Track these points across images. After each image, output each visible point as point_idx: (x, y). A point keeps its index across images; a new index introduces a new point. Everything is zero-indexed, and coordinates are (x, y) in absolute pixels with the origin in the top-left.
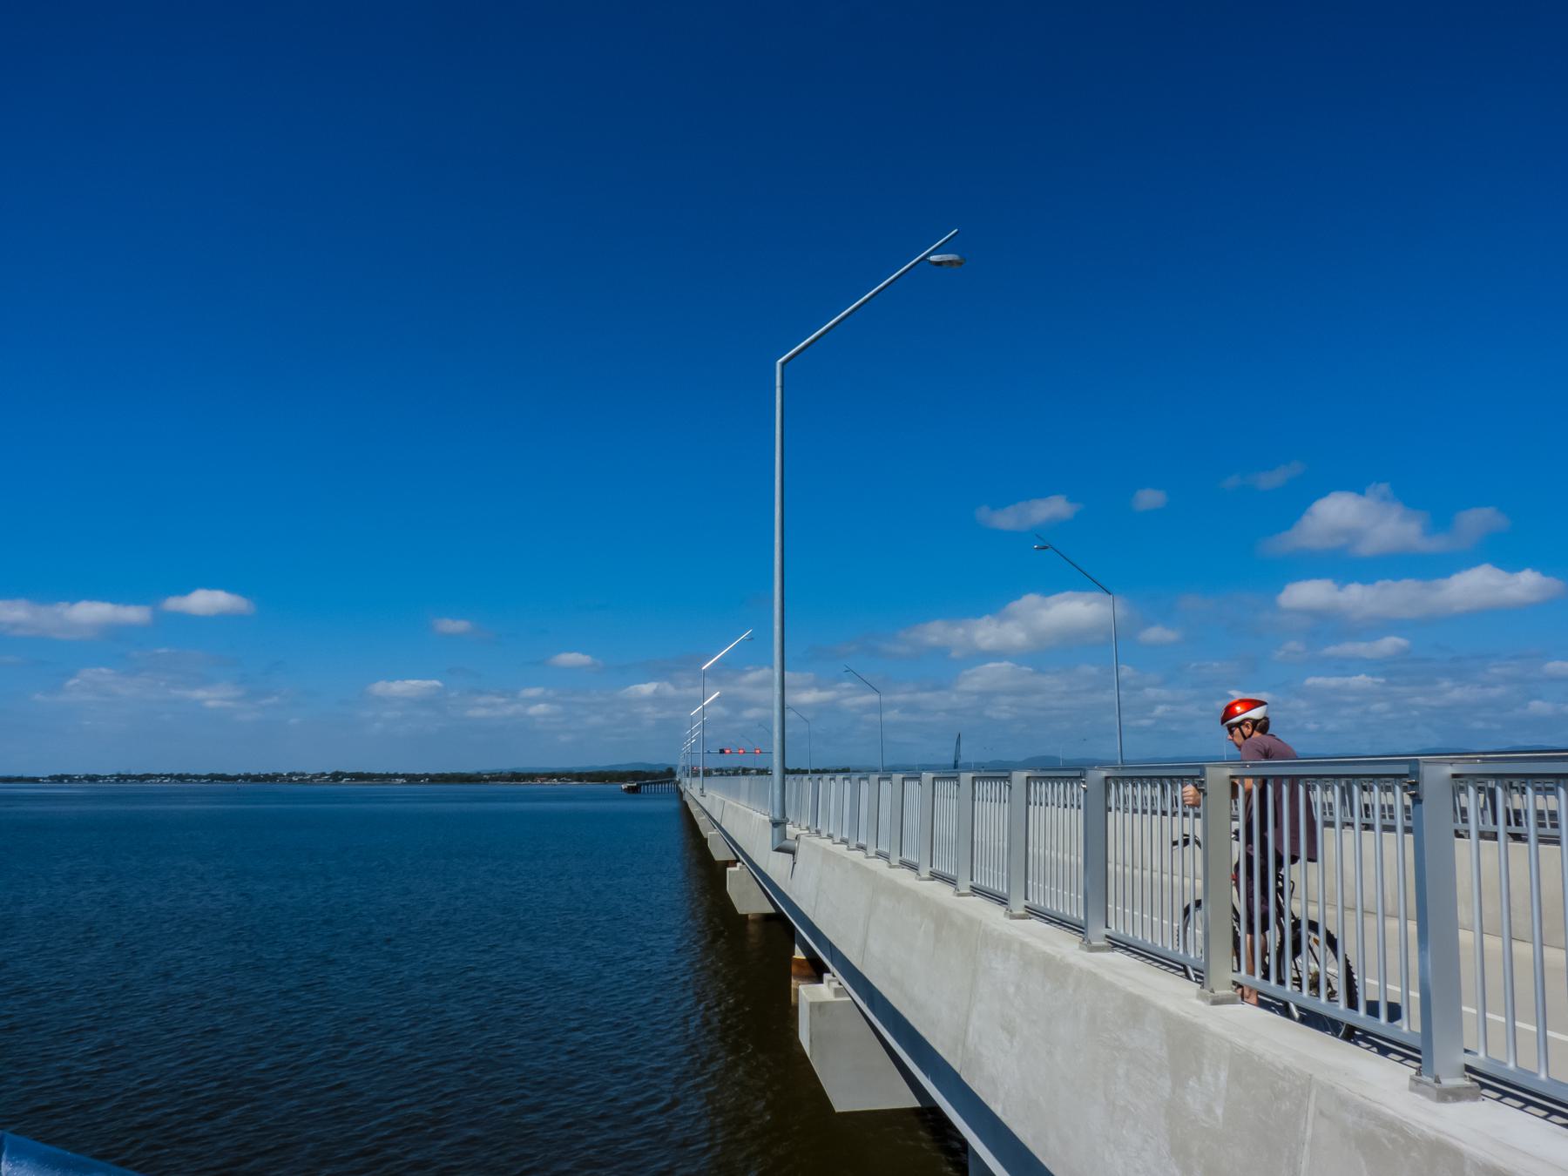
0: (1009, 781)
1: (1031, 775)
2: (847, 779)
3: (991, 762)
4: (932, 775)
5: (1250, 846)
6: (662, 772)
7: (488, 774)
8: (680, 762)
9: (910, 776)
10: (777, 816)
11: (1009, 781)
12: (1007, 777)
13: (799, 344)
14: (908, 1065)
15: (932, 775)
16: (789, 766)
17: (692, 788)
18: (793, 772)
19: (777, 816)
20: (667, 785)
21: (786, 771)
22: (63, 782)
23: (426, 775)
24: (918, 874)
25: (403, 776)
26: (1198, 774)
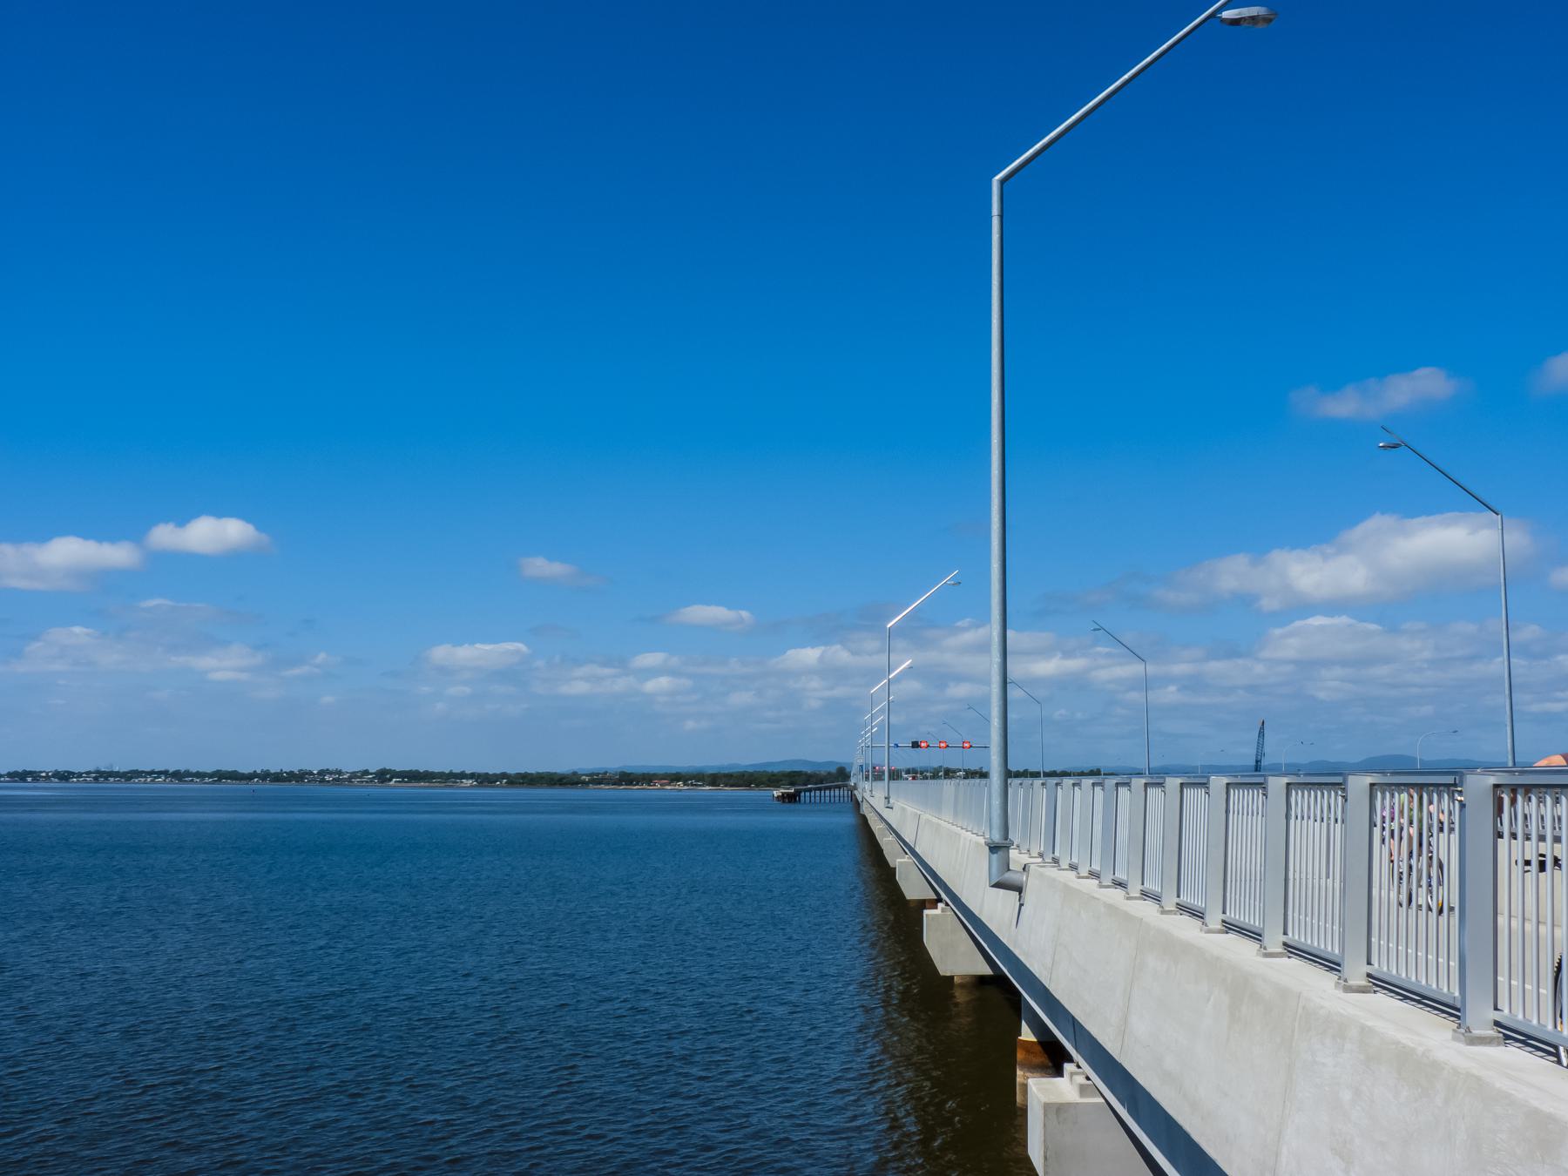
7: (587, 775)
17: (873, 796)
21: (1008, 774)
22: (25, 781)
23: (504, 775)
25: (472, 776)
26: (1262, 781)
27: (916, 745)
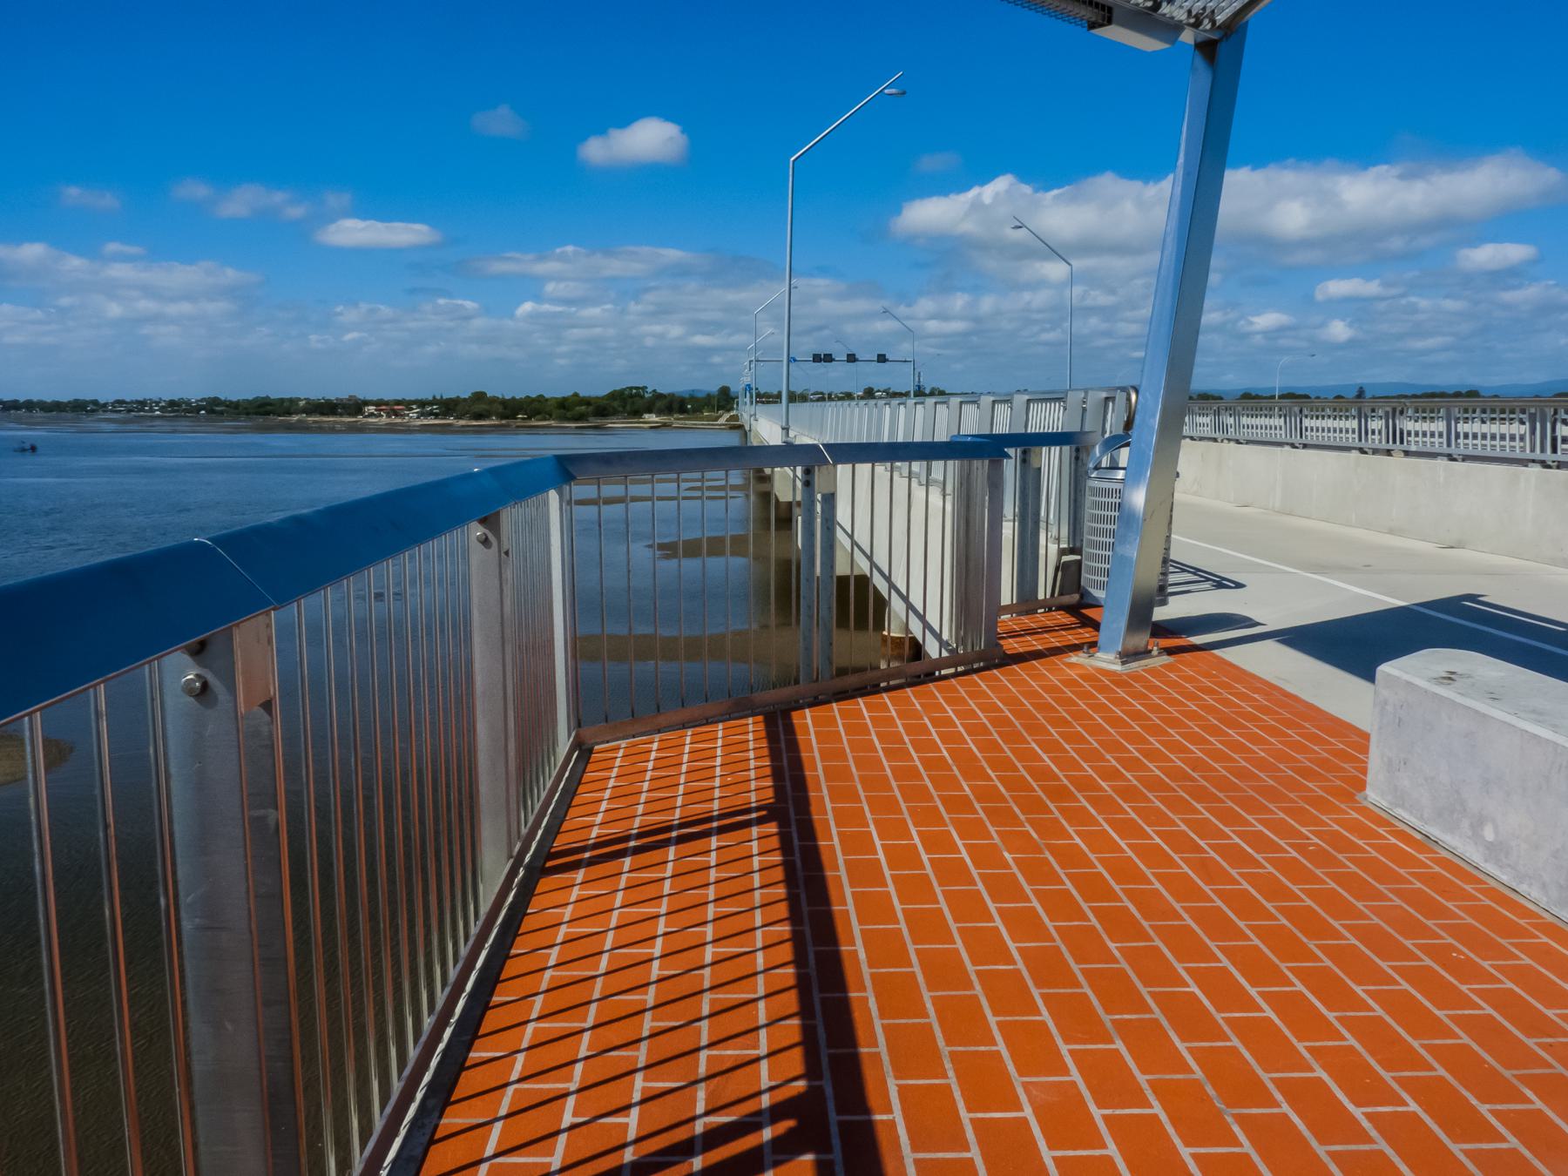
0: (1011, 403)
1: (962, 400)
2: (889, 404)
3: (378, 400)
4: (959, 399)
5: (1371, 451)
6: (709, 396)
8: (876, 363)
9: (966, 400)
10: (784, 424)
11: (1011, 403)
12: (1062, 398)
13: (75, 688)
14: (607, 940)
15: (959, 399)
16: (1203, 378)
18: (1208, 400)
19: (784, 424)
20: (643, 892)
24: (901, 474)
27: (882, 359)
